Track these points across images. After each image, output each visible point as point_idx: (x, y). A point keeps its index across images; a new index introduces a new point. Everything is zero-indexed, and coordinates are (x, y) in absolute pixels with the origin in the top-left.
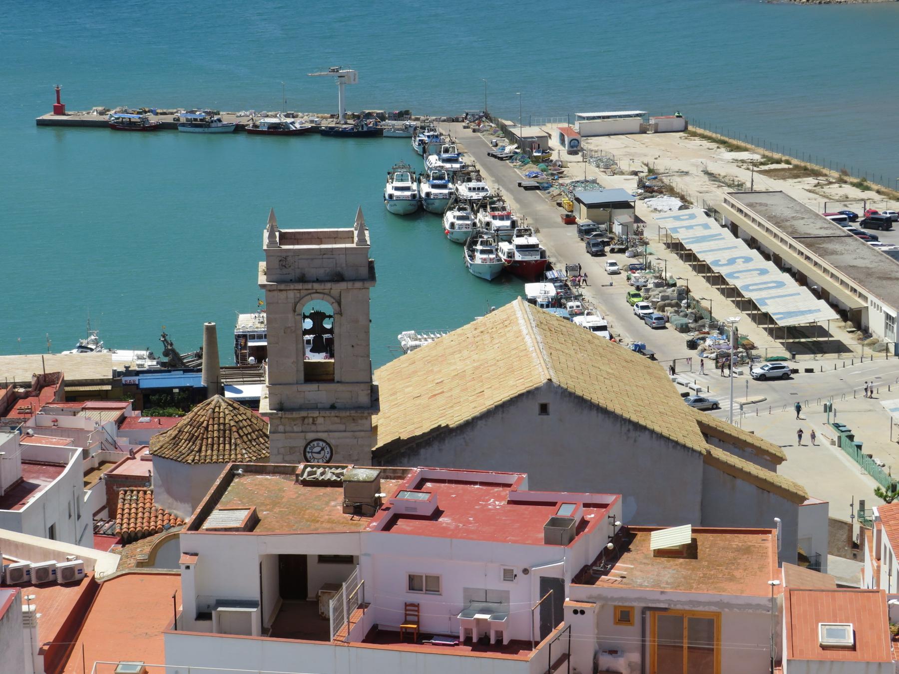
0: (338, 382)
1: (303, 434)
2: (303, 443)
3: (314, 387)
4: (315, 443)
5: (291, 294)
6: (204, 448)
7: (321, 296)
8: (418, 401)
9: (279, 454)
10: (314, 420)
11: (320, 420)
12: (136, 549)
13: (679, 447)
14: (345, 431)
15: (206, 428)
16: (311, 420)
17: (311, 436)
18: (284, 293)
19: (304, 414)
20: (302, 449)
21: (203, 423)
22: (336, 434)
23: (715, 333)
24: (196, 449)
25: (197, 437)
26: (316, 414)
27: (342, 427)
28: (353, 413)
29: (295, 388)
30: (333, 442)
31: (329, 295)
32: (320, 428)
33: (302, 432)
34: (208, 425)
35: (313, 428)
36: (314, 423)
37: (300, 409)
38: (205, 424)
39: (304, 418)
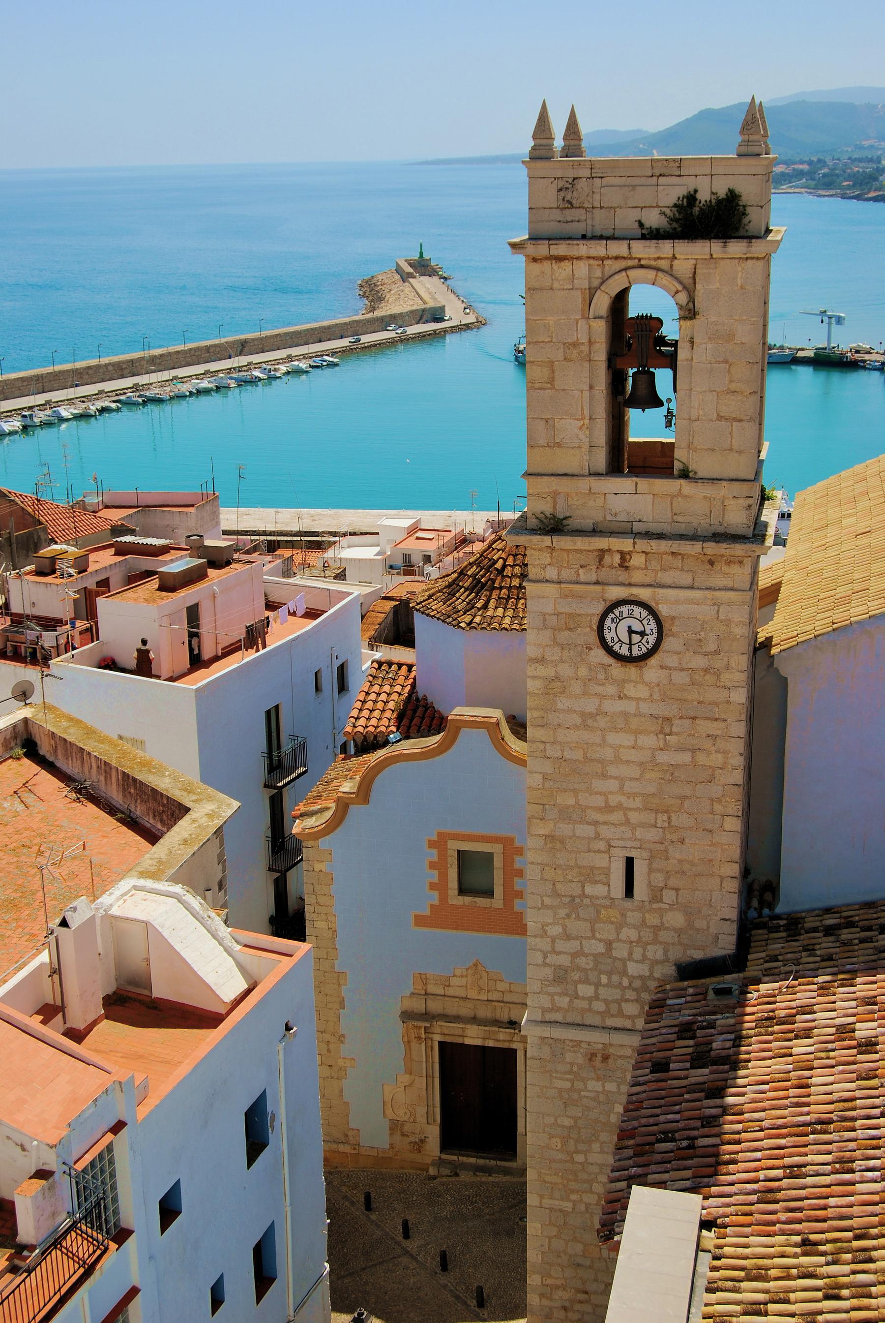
0: (685, 474)
1: (598, 588)
2: (600, 608)
3: (625, 484)
4: (625, 609)
5: (582, 269)
6: (492, 604)
7: (651, 274)
8: (863, 541)
9: (545, 627)
10: (623, 559)
11: (637, 560)
12: (210, 799)
13: (590, 527)
14: (692, 588)
15: (500, 572)
16: (617, 559)
17: (616, 593)
18: (566, 264)
19: (602, 543)
20: (595, 620)
21: (496, 562)
22: (671, 592)
23: (364, 1266)
24: (479, 605)
25: (484, 585)
26: (626, 544)
27: (686, 579)
28: (711, 548)
29: (584, 484)
30: (663, 610)
31: (670, 273)
32: (637, 577)
33: (597, 583)
34: (504, 566)
35: (622, 576)
36: (624, 565)
37: (595, 531)
38: (499, 565)
39: (602, 553)
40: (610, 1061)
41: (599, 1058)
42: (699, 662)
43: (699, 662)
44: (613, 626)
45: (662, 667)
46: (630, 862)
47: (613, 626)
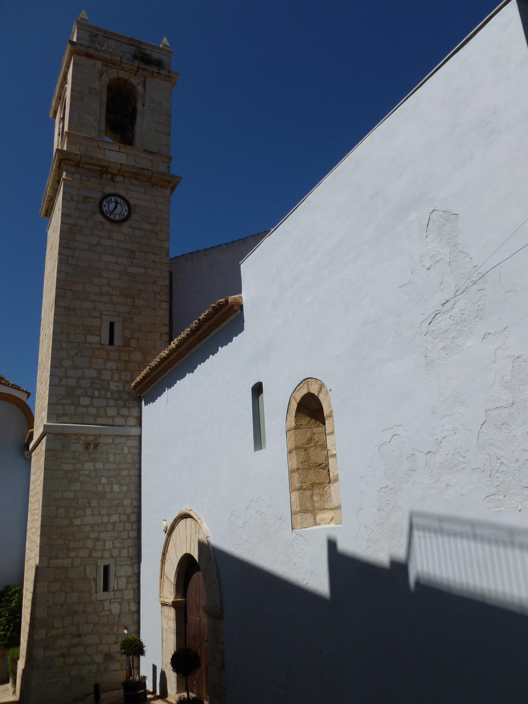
10: (112, 177)
17: (109, 190)
30: (131, 202)
40: (99, 447)
41: (92, 446)
42: (148, 227)
43: (148, 227)
44: (107, 205)
45: (130, 227)
46: (112, 325)
47: (107, 205)
